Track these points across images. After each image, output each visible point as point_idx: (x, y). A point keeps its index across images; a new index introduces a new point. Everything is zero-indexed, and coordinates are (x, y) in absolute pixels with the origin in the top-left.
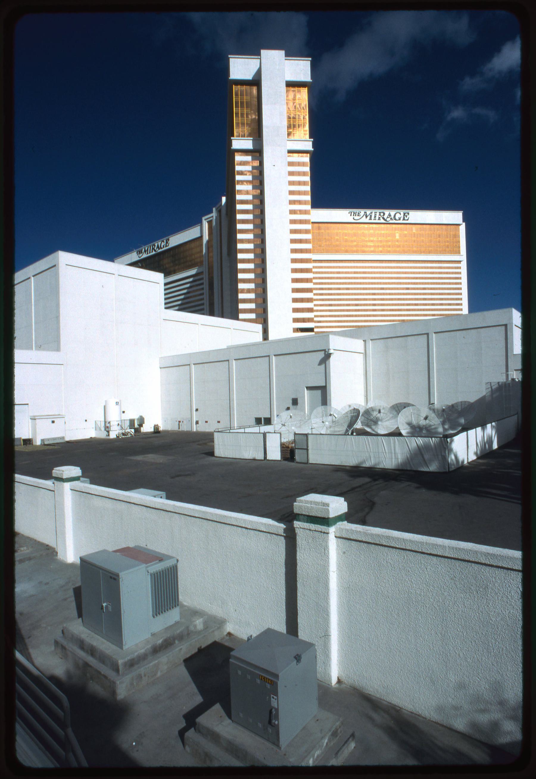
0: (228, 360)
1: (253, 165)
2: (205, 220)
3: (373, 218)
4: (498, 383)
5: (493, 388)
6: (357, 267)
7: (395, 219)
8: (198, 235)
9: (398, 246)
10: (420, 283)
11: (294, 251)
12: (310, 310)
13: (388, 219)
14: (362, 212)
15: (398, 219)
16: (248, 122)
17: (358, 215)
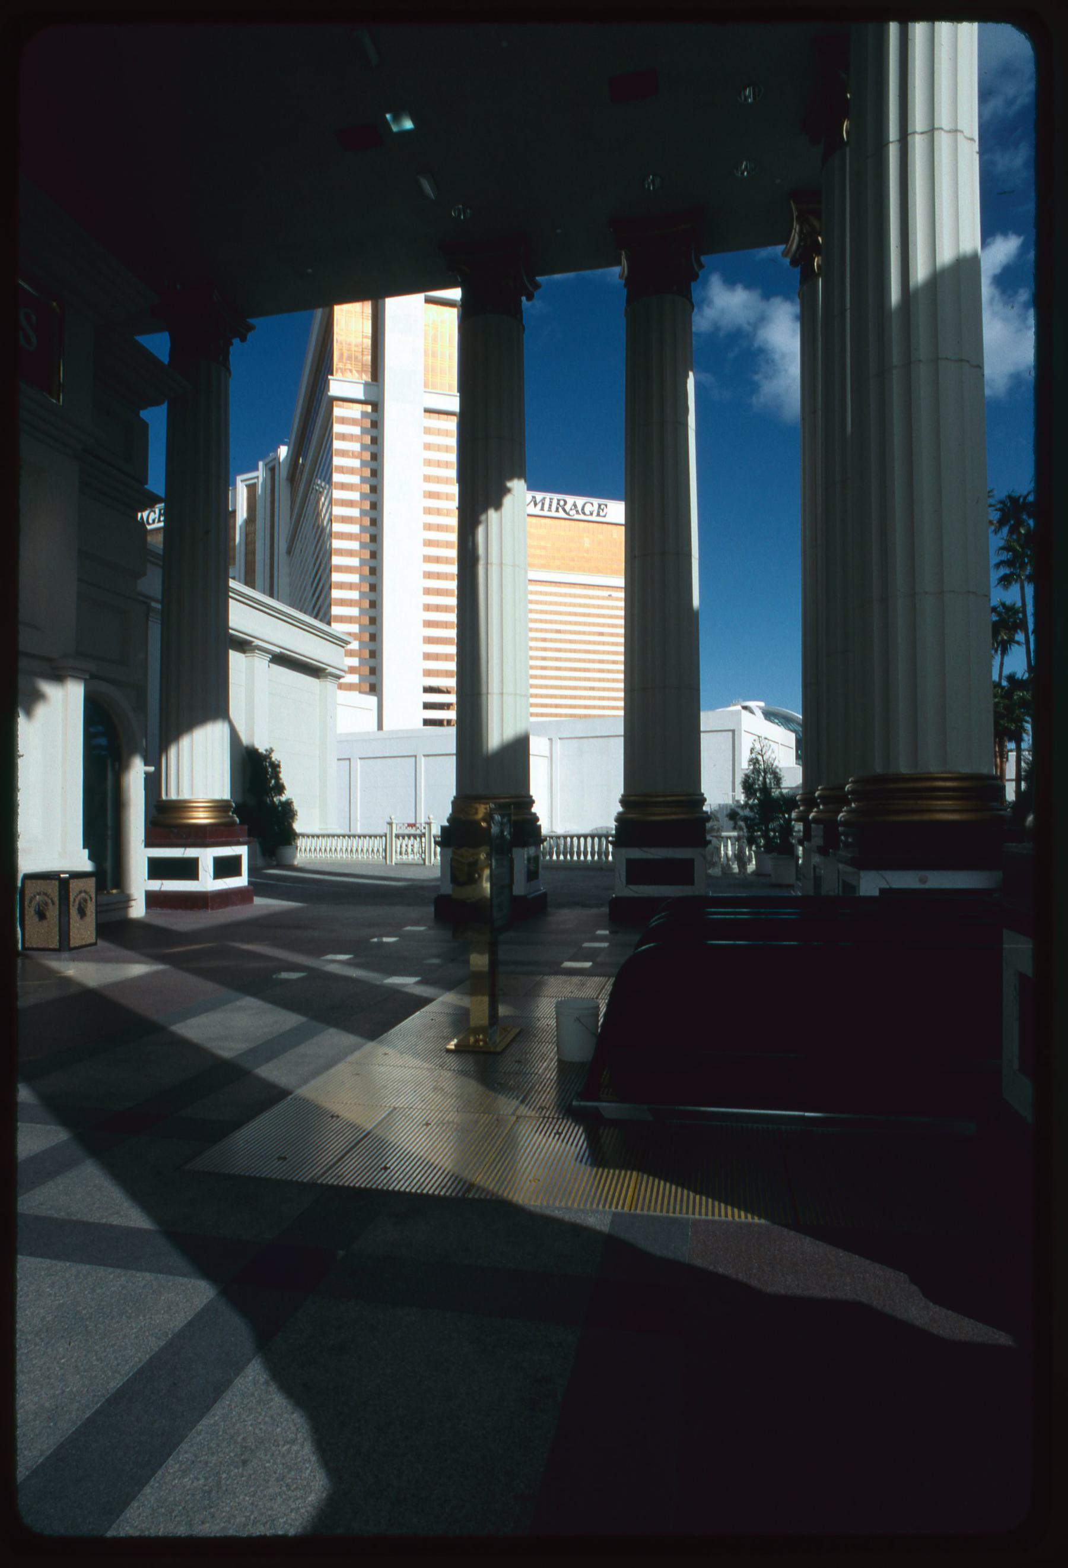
2: (242, 481)
4: (719, 805)
7: (584, 514)
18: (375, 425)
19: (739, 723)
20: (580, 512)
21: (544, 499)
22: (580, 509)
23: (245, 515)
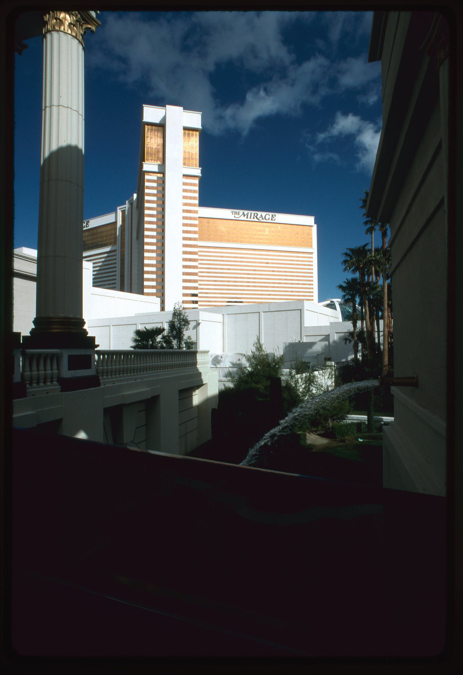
0: (136, 324)
1: (158, 176)
2: (119, 209)
3: (249, 217)
4: (289, 343)
5: (287, 345)
6: (236, 253)
7: (266, 219)
8: (114, 221)
9: (267, 239)
10: (283, 268)
11: (185, 246)
12: (196, 288)
13: (260, 219)
14: (241, 212)
15: (268, 219)
16: (155, 152)
17: (238, 215)
18: (162, 183)
19: (303, 306)
20: (264, 218)
21: (248, 213)
22: (264, 217)
23: (121, 223)
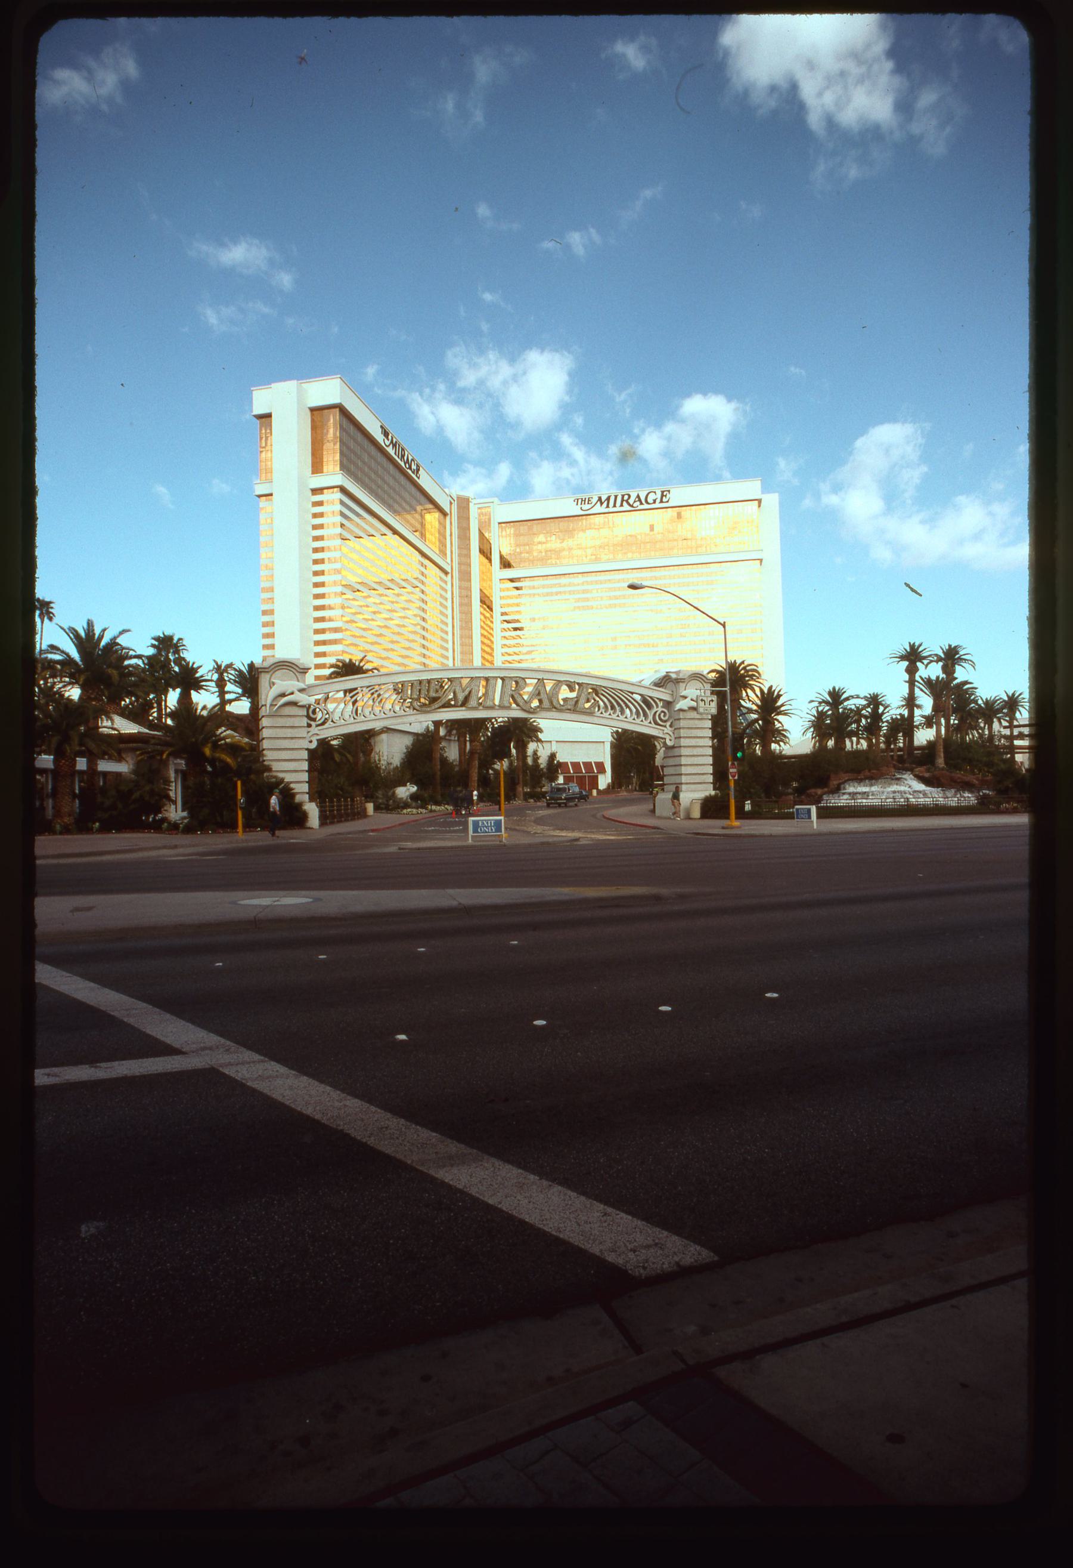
7: (649, 504)
13: (635, 505)
15: (652, 502)
